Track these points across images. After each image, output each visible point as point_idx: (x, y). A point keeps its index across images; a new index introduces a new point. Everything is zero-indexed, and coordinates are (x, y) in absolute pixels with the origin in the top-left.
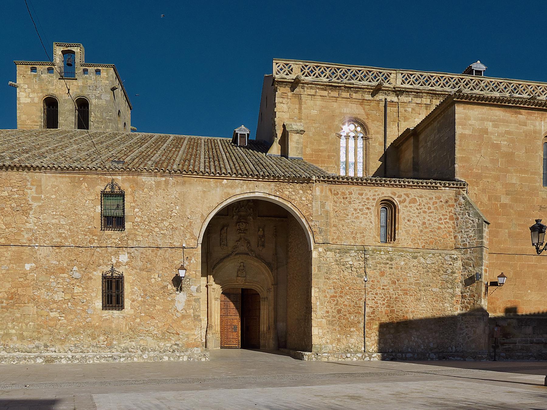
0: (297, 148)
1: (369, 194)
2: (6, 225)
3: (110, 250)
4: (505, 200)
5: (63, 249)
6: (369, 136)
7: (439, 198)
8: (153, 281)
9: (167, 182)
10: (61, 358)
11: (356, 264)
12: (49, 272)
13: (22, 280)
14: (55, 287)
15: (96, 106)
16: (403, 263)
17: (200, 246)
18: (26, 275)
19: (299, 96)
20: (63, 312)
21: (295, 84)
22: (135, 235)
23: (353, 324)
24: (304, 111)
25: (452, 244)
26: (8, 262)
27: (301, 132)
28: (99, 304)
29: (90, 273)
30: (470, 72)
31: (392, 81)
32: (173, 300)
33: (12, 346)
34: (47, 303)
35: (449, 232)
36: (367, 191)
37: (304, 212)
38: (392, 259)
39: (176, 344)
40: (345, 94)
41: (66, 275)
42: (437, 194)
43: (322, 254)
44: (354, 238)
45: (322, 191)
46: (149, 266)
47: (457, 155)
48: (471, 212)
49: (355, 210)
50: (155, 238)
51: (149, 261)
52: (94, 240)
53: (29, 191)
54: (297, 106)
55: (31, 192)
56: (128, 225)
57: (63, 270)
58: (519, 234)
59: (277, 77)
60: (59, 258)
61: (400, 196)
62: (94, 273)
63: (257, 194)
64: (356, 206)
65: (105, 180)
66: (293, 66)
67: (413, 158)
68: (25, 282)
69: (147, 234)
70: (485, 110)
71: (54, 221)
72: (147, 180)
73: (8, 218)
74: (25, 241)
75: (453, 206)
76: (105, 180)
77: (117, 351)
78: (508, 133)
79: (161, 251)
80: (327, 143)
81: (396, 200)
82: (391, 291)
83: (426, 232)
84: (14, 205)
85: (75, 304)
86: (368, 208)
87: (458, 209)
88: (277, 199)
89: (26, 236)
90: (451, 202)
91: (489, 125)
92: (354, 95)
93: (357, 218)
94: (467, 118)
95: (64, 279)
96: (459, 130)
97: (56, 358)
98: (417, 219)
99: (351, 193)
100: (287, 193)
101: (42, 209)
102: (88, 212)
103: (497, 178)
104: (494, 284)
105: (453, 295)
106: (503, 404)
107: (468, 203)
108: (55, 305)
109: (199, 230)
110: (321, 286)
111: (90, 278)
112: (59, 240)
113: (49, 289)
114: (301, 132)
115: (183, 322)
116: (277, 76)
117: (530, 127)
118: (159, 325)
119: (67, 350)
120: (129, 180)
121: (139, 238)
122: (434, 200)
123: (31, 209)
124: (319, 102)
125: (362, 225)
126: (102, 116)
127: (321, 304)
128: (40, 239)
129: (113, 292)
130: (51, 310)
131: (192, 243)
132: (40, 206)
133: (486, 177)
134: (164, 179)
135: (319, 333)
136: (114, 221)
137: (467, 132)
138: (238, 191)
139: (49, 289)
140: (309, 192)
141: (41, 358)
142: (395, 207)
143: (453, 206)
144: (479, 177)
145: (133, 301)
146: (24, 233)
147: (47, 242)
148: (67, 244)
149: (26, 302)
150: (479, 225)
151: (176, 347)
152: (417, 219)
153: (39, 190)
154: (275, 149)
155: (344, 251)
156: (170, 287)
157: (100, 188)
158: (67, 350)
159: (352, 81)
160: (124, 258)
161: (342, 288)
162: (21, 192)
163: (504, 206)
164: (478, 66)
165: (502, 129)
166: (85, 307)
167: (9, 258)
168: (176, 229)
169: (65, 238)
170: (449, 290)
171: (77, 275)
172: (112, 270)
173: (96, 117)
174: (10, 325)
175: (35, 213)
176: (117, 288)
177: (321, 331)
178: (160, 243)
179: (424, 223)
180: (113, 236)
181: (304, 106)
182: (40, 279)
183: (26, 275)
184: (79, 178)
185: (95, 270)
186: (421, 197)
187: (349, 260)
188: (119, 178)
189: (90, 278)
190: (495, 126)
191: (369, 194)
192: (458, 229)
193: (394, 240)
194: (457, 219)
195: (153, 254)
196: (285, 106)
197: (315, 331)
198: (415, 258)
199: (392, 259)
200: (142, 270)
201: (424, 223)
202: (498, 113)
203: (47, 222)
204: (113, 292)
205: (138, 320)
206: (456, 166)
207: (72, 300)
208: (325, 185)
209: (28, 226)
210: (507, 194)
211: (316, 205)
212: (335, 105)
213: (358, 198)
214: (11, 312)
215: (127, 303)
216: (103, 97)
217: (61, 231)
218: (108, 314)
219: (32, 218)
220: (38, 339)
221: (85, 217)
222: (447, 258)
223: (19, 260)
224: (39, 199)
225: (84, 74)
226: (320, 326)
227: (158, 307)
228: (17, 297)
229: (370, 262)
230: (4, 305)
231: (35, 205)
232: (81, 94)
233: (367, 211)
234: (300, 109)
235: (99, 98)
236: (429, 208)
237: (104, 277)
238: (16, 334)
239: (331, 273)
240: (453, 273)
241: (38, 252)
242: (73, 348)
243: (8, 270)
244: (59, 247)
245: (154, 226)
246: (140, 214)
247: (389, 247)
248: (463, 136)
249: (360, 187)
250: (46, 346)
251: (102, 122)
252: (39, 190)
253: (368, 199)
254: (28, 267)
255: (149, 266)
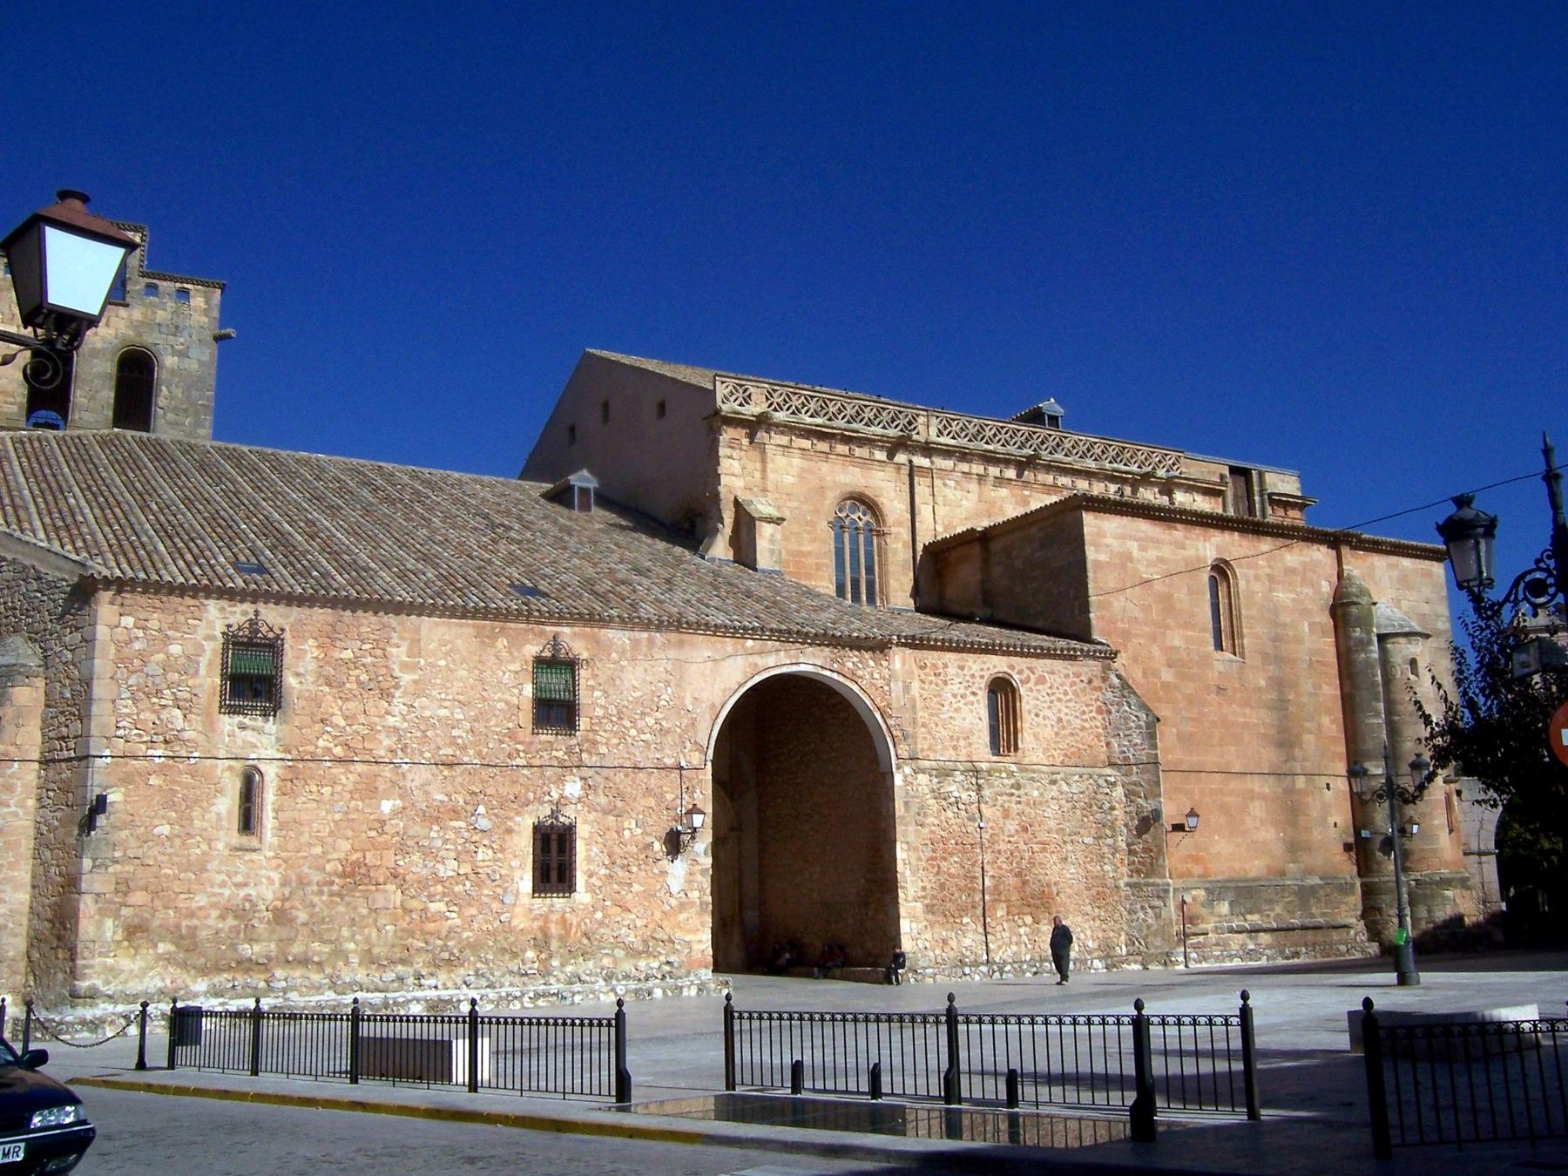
0: (772, 552)
1: (974, 667)
2: (346, 718)
3: (549, 772)
4: (1167, 676)
5: (459, 769)
6: (886, 530)
7: (1077, 675)
8: (627, 833)
9: (651, 641)
10: (459, 1001)
11: (964, 796)
12: (433, 817)
13: (373, 834)
14: (439, 850)
15: (173, 372)
16: (1036, 793)
17: (709, 764)
18: (383, 823)
19: (762, 449)
20: (453, 900)
21: (756, 426)
22: (595, 743)
23: (963, 910)
24: (771, 476)
25: (1103, 757)
26: (348, 796)
27: (779, 521)
28: (526, 882)
29: (510, 819)
30: (1036, 417)
31: (921, 428)
32: (664, 873)
33: (348, 980)
34: (423, 884)
35: (1098, 736)
36: (970, 663)
37: (878, 701)
38: (1018, 786)
39: (668, 963)
40: (842, 449)
41: (462, 824)
42: (1075, 669)
43: (910, 779)
44: (955, 748)
45: (903, 664)
46: (619, 804)
47: (1092, 599)
48: (1133, 700)
49: (955, 696)
50: (632, 749)
51: (620, 795)
52: (518, 751)
53: (394, 650)
54: (758, 465)
55: (399, 653)
56: (583, 723)
57: (456, 813)
58: (1192, 735)
59: (726, 408)
60: (450, 789)
61: (1020, 672)
62: (518, 819)
63: (803, 668)
64: (955, 688)
65: (542, 633)
66: (752, 390)
67: (982, 582)
68: (381, 839)
69: (615, 741)
70: (1125, 521)
71: (443, 712)
72: (617, 637)
73: (351, 705)
74: (382, 753)
75: (1100, 689)
76: (542, 633)
77: (558, 981)
78: (1161, 560)
79: (641, 775)
80: (813, 540)
81: (1016, 678)
82: (1022, 847)
83: (1065, 737)
84: (364, 677)
85: (479, 885)
86: (974, 694)
87: (1109, 695)
88: (835, 676)
89: (386, 742)
90: (1097, 683)
91: (1133, 546)
92: (858, 451)
93: (958, 710)
94: (1100, 534)
95: (457, 831)
96: (1091, 554)
97: (450, 1001)
98: (1048, 713)
99: (945, 666)
100: (850, 665)
101: (419, 689)
102: (507, 696)
103: (1153, 638)
104: (1178, 828)
105: (1115, 850)
106: (1468, 1014)
107: (1125, 685)
108: (439, 888)
109: (708, 731)
110: (911, 838)
111: (509, 831)
112: (450, 751)
113: (428, 853)
114: (779, 521)
115: (682, 917)
116: (724, 407)
117: (1191, 552)
118: (639, 923)
119: (459, 982)
120: (583, 636)
121: (603, 749)
122: (1071, 679)
123: (397, 687)
124: (797, 461)
125: (966, 724)
126: (189, 397)
127: (913, 874)
128: (413, 750)
129: (554, 861)
130: (431, 898)
131: (696, 759)
132: (415, 682)
133: (1137, 636)
134: (645, 635)
135: (914, 931)
136: (556, 711)
137: (1103, 558)
138: (771, 660)
139: (428, 853)
140: (885, 663)
141: (418, 1001)
142: (1014, 690)
143: (1100, 689)
144: (1126, 635)
145: (591, 876)
146: (382, 736)
147: (428, 755)
148: (466, 759)
149: (381, 880)
150: (1148, 726)
151: (667, 968)
152: (1048, 713)
153: (415, 649)
154: (721, 548)
155: (944, 773)
156: (657, 846)
157: (532, 650)
158: (459, 982)
159: (854, 426)
160: (573, 788)
161: (944, 841)
162: (379, 652)
163: (1166, 686)
164: (1050, 406)
165: (1152, 554)
166: (499, 890)
167: (350, 787)
168: (668, 731)
169: (464, 748)
170: (1109, 841)
171: (484, 823)
172: (554, 814)
173: (172, 397)
174: (345, 932)
175: (405, 693)
176: (561, 850)
177: (914, 925)
178: (640, 758)
179: (1060, 720)
180: (554, 744)
181: (770, 466)
182: (411, 833)
183: (383, 823)
184: (493, 628)
185: (518, 814)
186: (1052, 673)
187: (952, 788)
188: (567, 630)
189: (509, 831)
190: (1142, 549)
191: (974, 667)
192: (1114, 730)
193: (1016, 749)
194: (1109, 712)
195: (628, 781)
196: (736, 464)
197: (905, 925)
198: (1054, 782)
199: (1018, 786)
200: (605, 813)
201: (1060, 720)
202: (1143, 526)
203: (427, 713)
204: (554, 861)
205: (599, 915)
206: (1092, 615)
207: (472, 876)
208: (908, 651)
209: (391, 721)
210: (1170, 666)
211: (897, 687)
212: (825, 467)
213: (958, 675)
214: (348, 904)
215: (580, 879)
216: (193, 353)
217: (455, 733)
218: (541, 904)
219: (398, 705)
220: (403, 962)
221: (501, 705)
222: (1101, 782)
223: (369, 790)
224: (415, 667)
225: (147, 294)
226: (914, 918)
227: (636, 888)
228: (363, 870)
229: (986, 792)
230: (335, 888)
231: (406, 678)
232: (137, 341)
233: (972, 698)
234: (764, 471)
235: (183, 355)
236: (1066, 693)
237: (537, 829)
238: (355, 952)
239: (925, 815)
240: (1112, 808)
241: (410, 776)
242: (472, 978)
243: (346, 813)
244: (450, 765)
245: (628, 724)
246: (602, 701)
247: (1008, 762)
248: (1097, 564)
249: (959, 656)
250: (419, 977)
251: (186, 411)
252: (415, 649)
253: (973, 676)
254: (387, 806)
255: (619, 804)
